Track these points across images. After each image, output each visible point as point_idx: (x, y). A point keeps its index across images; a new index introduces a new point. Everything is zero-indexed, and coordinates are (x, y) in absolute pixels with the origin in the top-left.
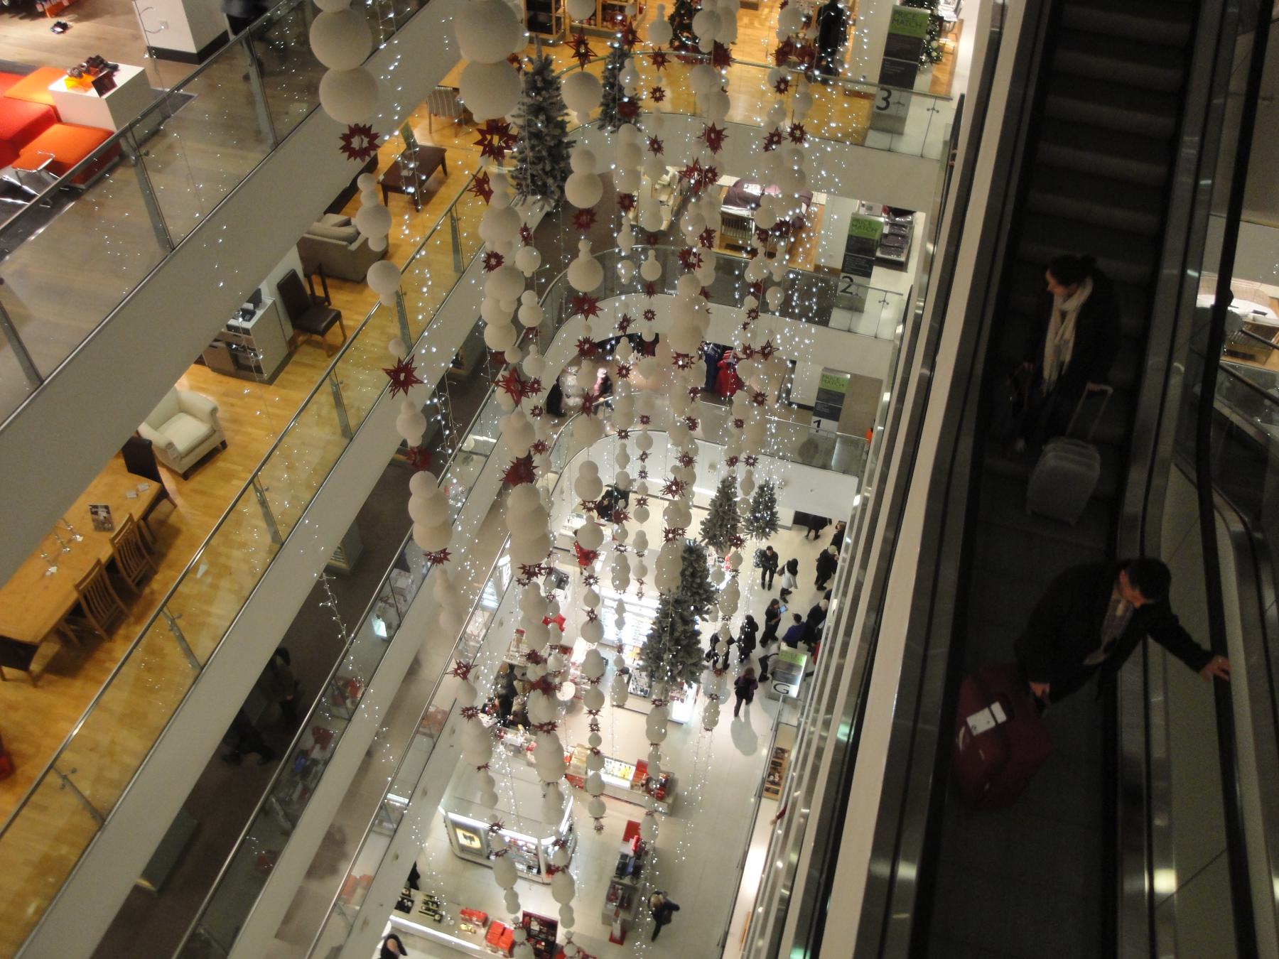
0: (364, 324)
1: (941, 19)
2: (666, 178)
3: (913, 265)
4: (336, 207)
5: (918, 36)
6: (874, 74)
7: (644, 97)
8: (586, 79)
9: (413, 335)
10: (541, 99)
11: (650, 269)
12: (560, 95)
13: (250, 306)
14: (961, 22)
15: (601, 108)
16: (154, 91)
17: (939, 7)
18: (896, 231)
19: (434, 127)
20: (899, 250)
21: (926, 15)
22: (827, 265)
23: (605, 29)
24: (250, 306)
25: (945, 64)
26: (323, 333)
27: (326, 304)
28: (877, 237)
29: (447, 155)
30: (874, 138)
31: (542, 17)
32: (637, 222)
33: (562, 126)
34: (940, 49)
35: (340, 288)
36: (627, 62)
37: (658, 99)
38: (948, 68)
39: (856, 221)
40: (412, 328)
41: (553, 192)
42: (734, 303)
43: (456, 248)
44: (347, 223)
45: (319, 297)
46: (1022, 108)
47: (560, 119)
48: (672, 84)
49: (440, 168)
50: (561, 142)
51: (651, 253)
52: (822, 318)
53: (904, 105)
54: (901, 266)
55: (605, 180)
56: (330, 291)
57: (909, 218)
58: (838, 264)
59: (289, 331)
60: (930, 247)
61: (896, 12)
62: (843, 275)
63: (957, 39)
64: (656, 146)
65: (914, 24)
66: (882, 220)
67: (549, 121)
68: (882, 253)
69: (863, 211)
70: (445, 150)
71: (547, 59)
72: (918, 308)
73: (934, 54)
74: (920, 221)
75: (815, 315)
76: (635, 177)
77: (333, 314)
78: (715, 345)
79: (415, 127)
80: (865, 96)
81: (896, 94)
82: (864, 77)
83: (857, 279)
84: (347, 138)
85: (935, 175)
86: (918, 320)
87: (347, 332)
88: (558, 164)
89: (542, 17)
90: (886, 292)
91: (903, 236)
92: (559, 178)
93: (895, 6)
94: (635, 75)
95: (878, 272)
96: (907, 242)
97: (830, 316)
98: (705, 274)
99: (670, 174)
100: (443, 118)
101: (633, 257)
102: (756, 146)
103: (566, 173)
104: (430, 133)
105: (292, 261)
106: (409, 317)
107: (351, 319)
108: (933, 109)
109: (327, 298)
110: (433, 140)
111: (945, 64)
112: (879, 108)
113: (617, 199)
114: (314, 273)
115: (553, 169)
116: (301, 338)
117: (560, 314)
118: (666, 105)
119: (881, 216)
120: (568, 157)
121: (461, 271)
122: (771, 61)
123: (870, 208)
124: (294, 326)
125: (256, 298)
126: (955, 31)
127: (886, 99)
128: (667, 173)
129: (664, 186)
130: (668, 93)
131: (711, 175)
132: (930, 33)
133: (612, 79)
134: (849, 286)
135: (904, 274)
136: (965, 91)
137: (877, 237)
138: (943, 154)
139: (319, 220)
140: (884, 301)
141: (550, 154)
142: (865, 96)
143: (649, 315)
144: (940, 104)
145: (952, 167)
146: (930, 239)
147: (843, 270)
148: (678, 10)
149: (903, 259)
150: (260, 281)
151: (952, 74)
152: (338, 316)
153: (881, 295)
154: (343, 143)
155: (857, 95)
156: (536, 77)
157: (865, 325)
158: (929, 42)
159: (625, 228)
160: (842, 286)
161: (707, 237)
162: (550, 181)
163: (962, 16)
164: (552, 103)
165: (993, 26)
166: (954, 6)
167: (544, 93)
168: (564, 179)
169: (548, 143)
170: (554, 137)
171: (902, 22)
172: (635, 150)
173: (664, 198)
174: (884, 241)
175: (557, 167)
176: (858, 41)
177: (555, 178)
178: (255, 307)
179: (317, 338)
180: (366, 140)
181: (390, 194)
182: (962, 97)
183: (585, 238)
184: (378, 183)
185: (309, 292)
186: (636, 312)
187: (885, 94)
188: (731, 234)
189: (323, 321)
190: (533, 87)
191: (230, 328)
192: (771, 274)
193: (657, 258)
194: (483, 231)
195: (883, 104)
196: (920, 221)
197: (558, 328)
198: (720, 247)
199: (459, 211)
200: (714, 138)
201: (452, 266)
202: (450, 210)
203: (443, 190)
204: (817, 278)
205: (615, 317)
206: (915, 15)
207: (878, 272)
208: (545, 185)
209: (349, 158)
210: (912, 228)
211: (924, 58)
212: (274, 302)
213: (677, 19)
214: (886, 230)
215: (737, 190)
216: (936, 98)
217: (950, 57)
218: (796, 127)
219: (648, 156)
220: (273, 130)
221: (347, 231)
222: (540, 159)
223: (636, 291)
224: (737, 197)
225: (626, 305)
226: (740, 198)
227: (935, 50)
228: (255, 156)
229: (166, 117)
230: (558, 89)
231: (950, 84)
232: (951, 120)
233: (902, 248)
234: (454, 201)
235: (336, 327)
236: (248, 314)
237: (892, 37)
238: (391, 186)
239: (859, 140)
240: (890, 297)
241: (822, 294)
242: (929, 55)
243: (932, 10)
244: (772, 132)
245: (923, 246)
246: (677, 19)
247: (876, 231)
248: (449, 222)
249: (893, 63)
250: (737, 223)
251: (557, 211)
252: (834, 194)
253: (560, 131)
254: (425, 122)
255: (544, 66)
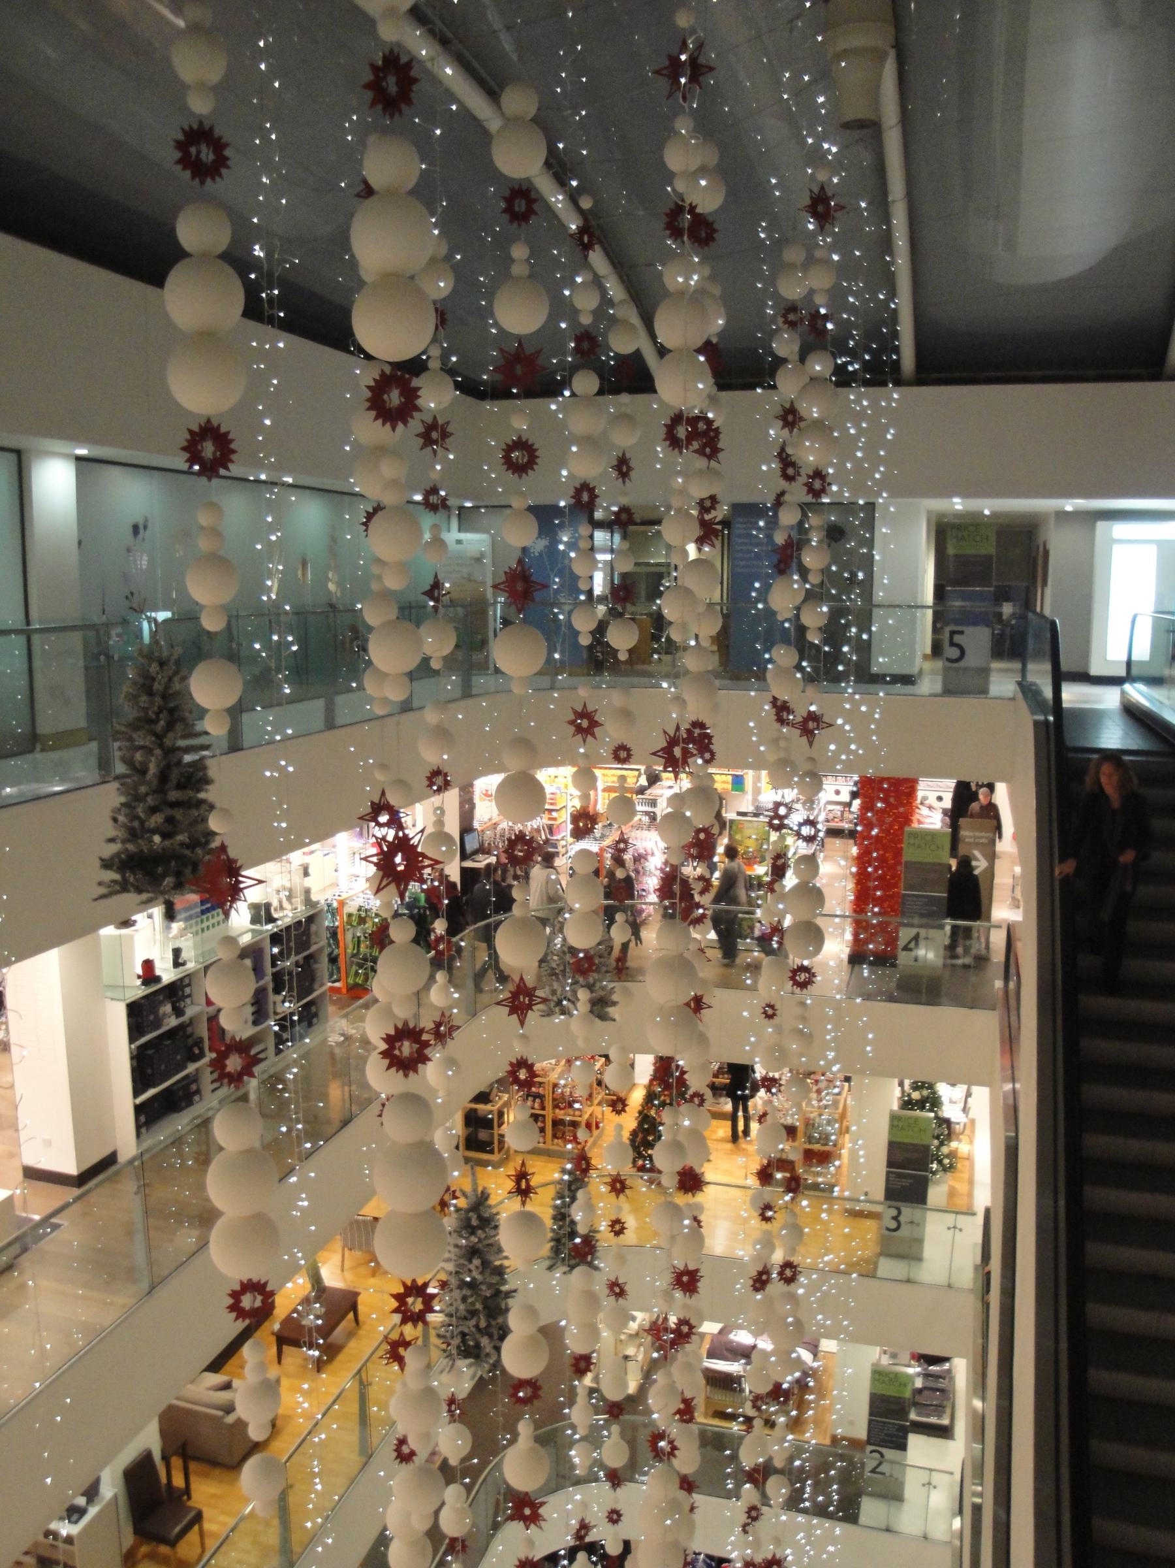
0: (232, 1530)
1: (948, 1122)
2: (633, 1326)
3: (961, 1428)
4: (215, 1366)
5: (925, 1143)
6: (878, 1190)
7: (602, 1228)
8: (528, 1220)
9: (296, 1548)
10: (476, 1240)
11: (614, 1452)
12: (509, 1148)
13: (81, 1501)
14: (973, 1122)
15: (552, 1244)
16: (18, 1217)
17: (944, 1108)
18: (931, 1384)
19: (347, 1264)
20: (939, 1410)
21: (929, 1119)
22: (845, 1435)
23: (558, 1148)
24: (81, 1501)
25: (962, 1172)
26: (173, 1543)
27: (185, 1497)
28: (908, 1394)
29: (360, 1299)
30: (887, 1267)
31: (483, 1135)
32: (598, 1383)
33: (500, 1272)
34: (952, 1155)
35: (206, 1475)
36: (580, 1194)
37: (618, 1233)
38: (966, 1176)
39: (878, 1374)
40: (296, 1537)
41: (488, 1355)
42: (728, 1495)
43: (364, 1418)
44: (227, 1386)
45: (178, 1489)
46: (1057, 1362)
47: (497, 1263)
48: (637, 1210)
49: (351, 1315)
50: (498, 1293)
51: (615, 1429)
52: (848, 1512)
53: (918, 1224)
54: (944, 1432)
55: (551, 1334)
56: (192, 1478)
57: (947, 1366)
58: (862, 1433)
59: (129, 1539)
60: (978, 1404)
61: (894, 1118)
62: (869, 1448)
63: (971, 1142)
64: (617, 1290)
65: (934, 847)
66: (911, 1371)
67: (485, 1264)
68: (919, 1414)
69: (885, 1361)
70: (357, 1294)
71: (483, 1192)
72: (975, 1494)
73: (946, 1161)
74: (961, 1369)
75: (838, 1510)
76: (592, 1332)
77: (192, 1514)
78: (708, 1556)
79: (324, 1263)
80: (870, 1215)
81: (908, 1212)
82: (866, 1194)
83: (889, 1454)
84: (236, 1296)
85: (969, 1306)
86: (977, 1509)
87: (207, 1541)
88: (495, 1319)
89: (483, 1135)
90: (931, 1470)
91: (942, 1391)
92: (496, 1337)
93: (891, 1111)
94: (590, 1207)
95: (915, 1441)
96: (948, 1399)
97: (858, 1509)
98: (688, 1460)
99: (638, 1321)
100: (359, 1254)
101: (593, 1439)
102: (742, 1286)
103: (504, 1332)
104: (342, 1270)
105: (149, 1439)
106: (294, 1518)
107: (215, 1523)
108: (955, 1227)
109: (187, 1491)
110: (345, 1280)
111: (962, 1172)
112: (888, 1229)
113: (569, 1361)
114: (175, 1454)
115: (489, 1326)
116: (144, 1549)
117: (496, 1515)
118: (630, 1237)
119: (909, 1366)
120: (507, 1310)
121: (367, 1454)
122: (753, 1182)
123: (894, 1356)
124: (138, 1531)
125: (92, 1493)
126: (967, 1132)
127: (895, 1218)
128: (634, 1319)
129: (631, 1336)
130: (631, 1222)
131: (684, 1333)
132: (938, 1137)
133: (561, 1216)
134: (880, 1464)
135: (950, 1443)
136: (988, 1203)
137: (908, 1394)
138: (975, 1280)
139: (192, 1382)
140: (929, 1484)
141: (486, 1307)
142: (870, 1215)
143: (614, 1517)
144: (962, 1220)
145: (989, 1273)
146: (975, 1394)
147: (869, 1442)
148: (641, 1124)
149: (945, 1421)
150: (102, 1466)
151: (971, 1182)
152: (198, 1517)
153: (923, 1476)
154: (230, 1301)
155: (859, 1214)
156: (471, 1214)
157: (909, 1520)
158: (938, 1148)
159: (581, 1398)
160: (870, 1464)
161: (686, 1412)
162: (485, 1341)
163: (971, 1115)
164: (489, 1245)
165: (1006, 1131)
166: (962, 1105)
167: (479, 1232)
168: (502, 1338)
169: (484, 1294)
170: (490, 1286)
171: (902, 1129)
172: (591, 1300)
173: (630, 1351)
174: (918, 1399)
175: (493, 1323)
176: (853, 1153)
177: (491, 1336)
178: (88, 1503)
179: (164, 1549)
180: (259, 1298)
181: (285, 1348)
182: (988, 1212)
183: (663, 265)
184: (273, 1334)
185: (164, 1480)
186: (597, 1514)
187: (894, 1212)
188: (720, 1397)
189: (176, 1525)
190: (467, 1228)
191: (47, 1533)
192: (770, 1459)
193: (623, 1435)
194: (395, 1408)
195: (893, 1225)
196: (961, 1369)
197: (493, 1536)
198: (706, 1415)
199: (370, 1373)
200: (687, 1281)
201: (357, 1448)
202: (359, 1371)
203: (353, 1344)
204: (835, 1455)
205: (568, 1525)
206: (916, 1119)
207: (915, 1441)
208: (478, 1346)
209: (237, 1319)
210: (952, 1379)
211: (934, 1166)
212: (115, 1497)
213: (640, 1135)
214: (919, 1384)
215: (794, 566)
216: (957, 1213)
217: (967, 1163)
218: (788, 1265)
219: (608, 1302)
220: (150, 1264)
221: (224, 1396)
222: (473, 1313)
223: (597, 1480)
224: (723, 1349)
225: (584, 1505)
226: (727, 1349)
227: (947, 1156)
228: (123, 1299)
229: (25, 1250)
230: (496, 1227)
231: (970, 1195)
232: (978, 1238)
233: (944, 1407)
234: (365, 1358)
235: (193, 1536)
236: (74, 1513)
237: (892, 1146)
238: (283, 1340)
239: (869, 1273)
240: (936, 1478)
241: (846, 1478)
242: (940, 1162)
243: (936, 1112)
244: (760, 1269)
245: (969, 1403)
246: (640, 1135)
247: (905, 1385)
248: (357, 1386)
249: (900, 1176)
250: (724, 1383)
251: (495, 1375)
252: (843, 1340)
253: (498, 1278)
254: (336, 1258)
255: (481, 1201)
